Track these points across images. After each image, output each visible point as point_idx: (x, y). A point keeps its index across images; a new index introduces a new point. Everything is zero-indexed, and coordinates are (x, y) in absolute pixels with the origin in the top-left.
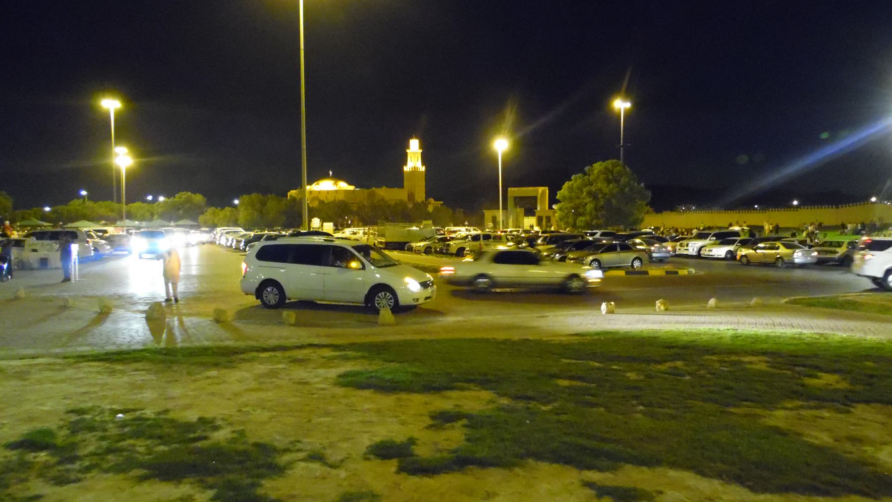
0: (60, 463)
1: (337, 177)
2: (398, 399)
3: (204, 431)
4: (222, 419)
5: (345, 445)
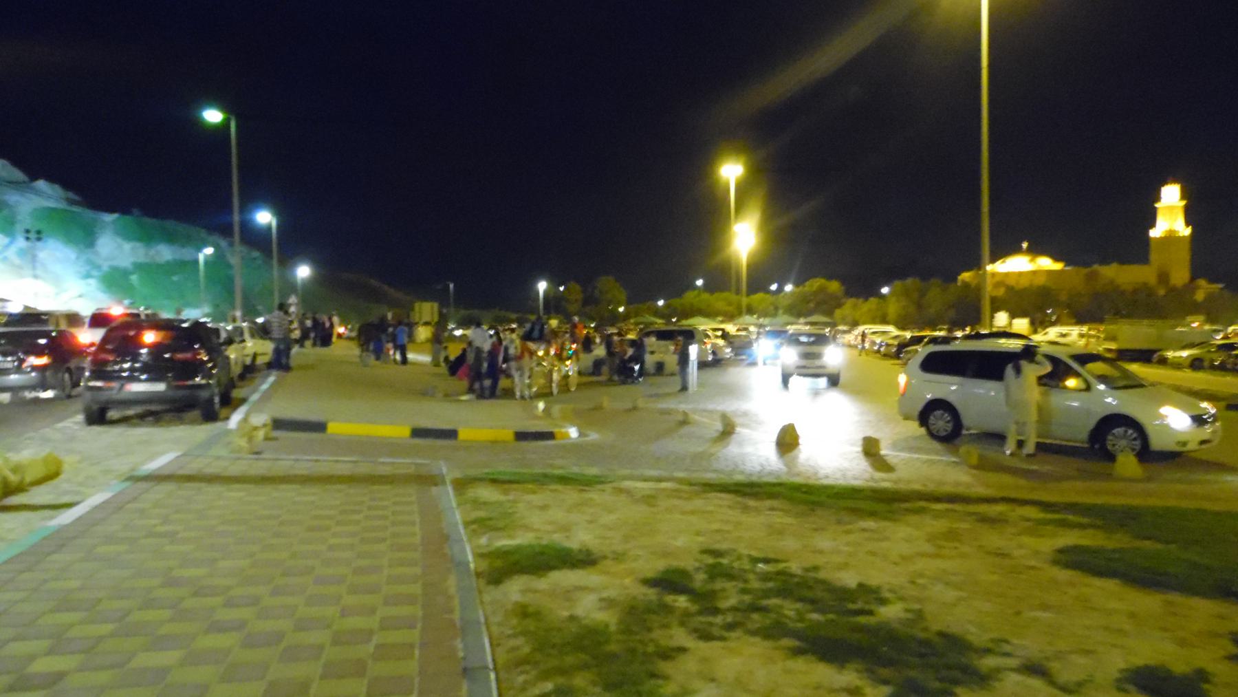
0: (700, 613)
1: (1035, 251)
2: (1170, 603)
3: (867, 603)
4: (890, 591)
5: (1081, 660)
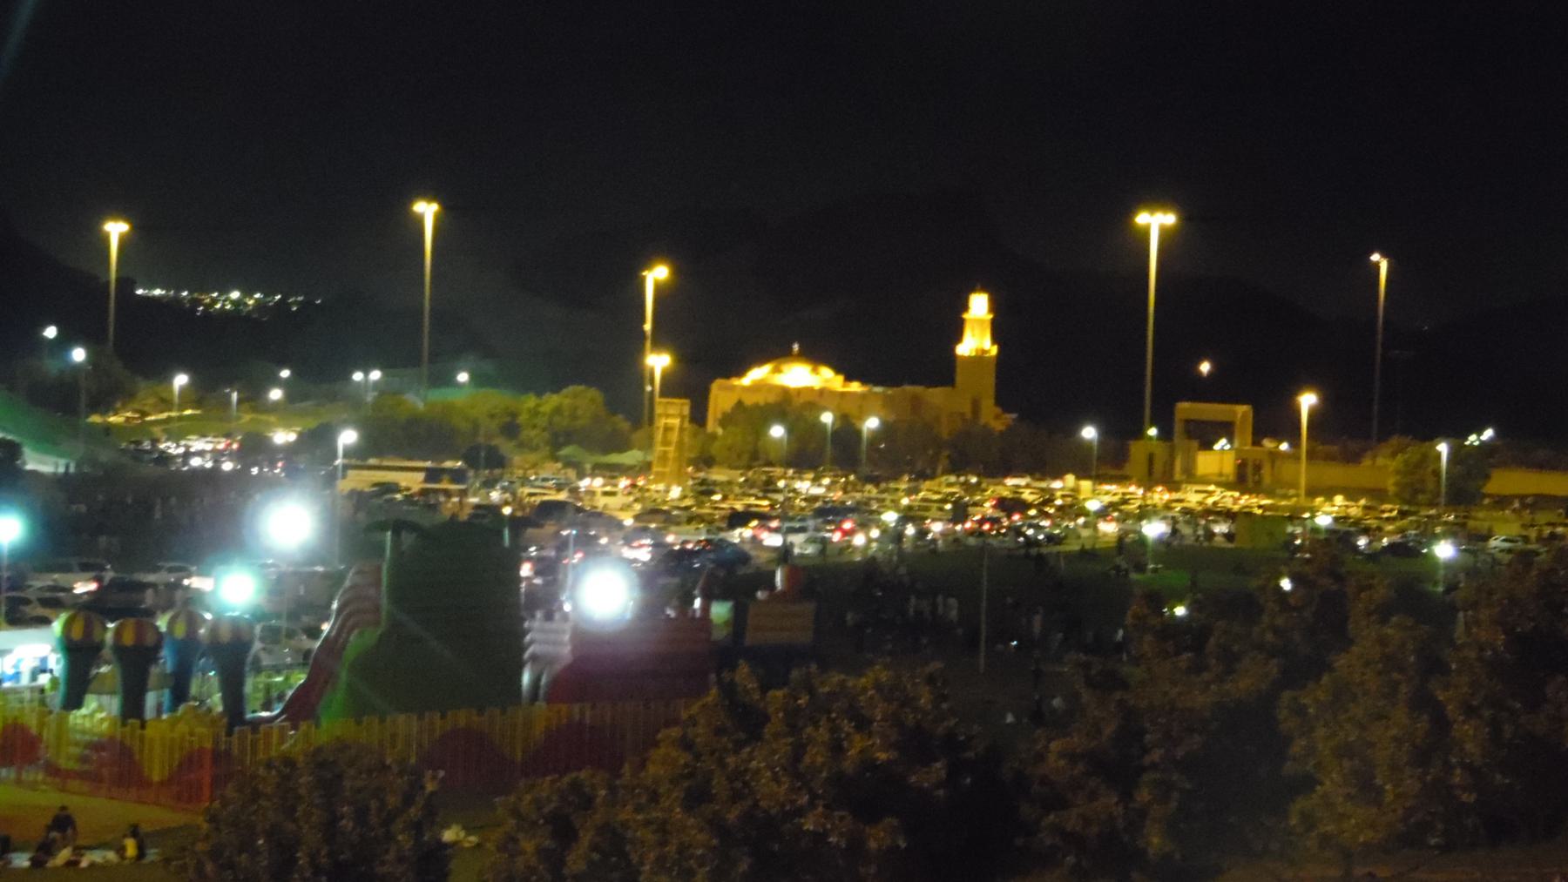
1: (814, 355)
